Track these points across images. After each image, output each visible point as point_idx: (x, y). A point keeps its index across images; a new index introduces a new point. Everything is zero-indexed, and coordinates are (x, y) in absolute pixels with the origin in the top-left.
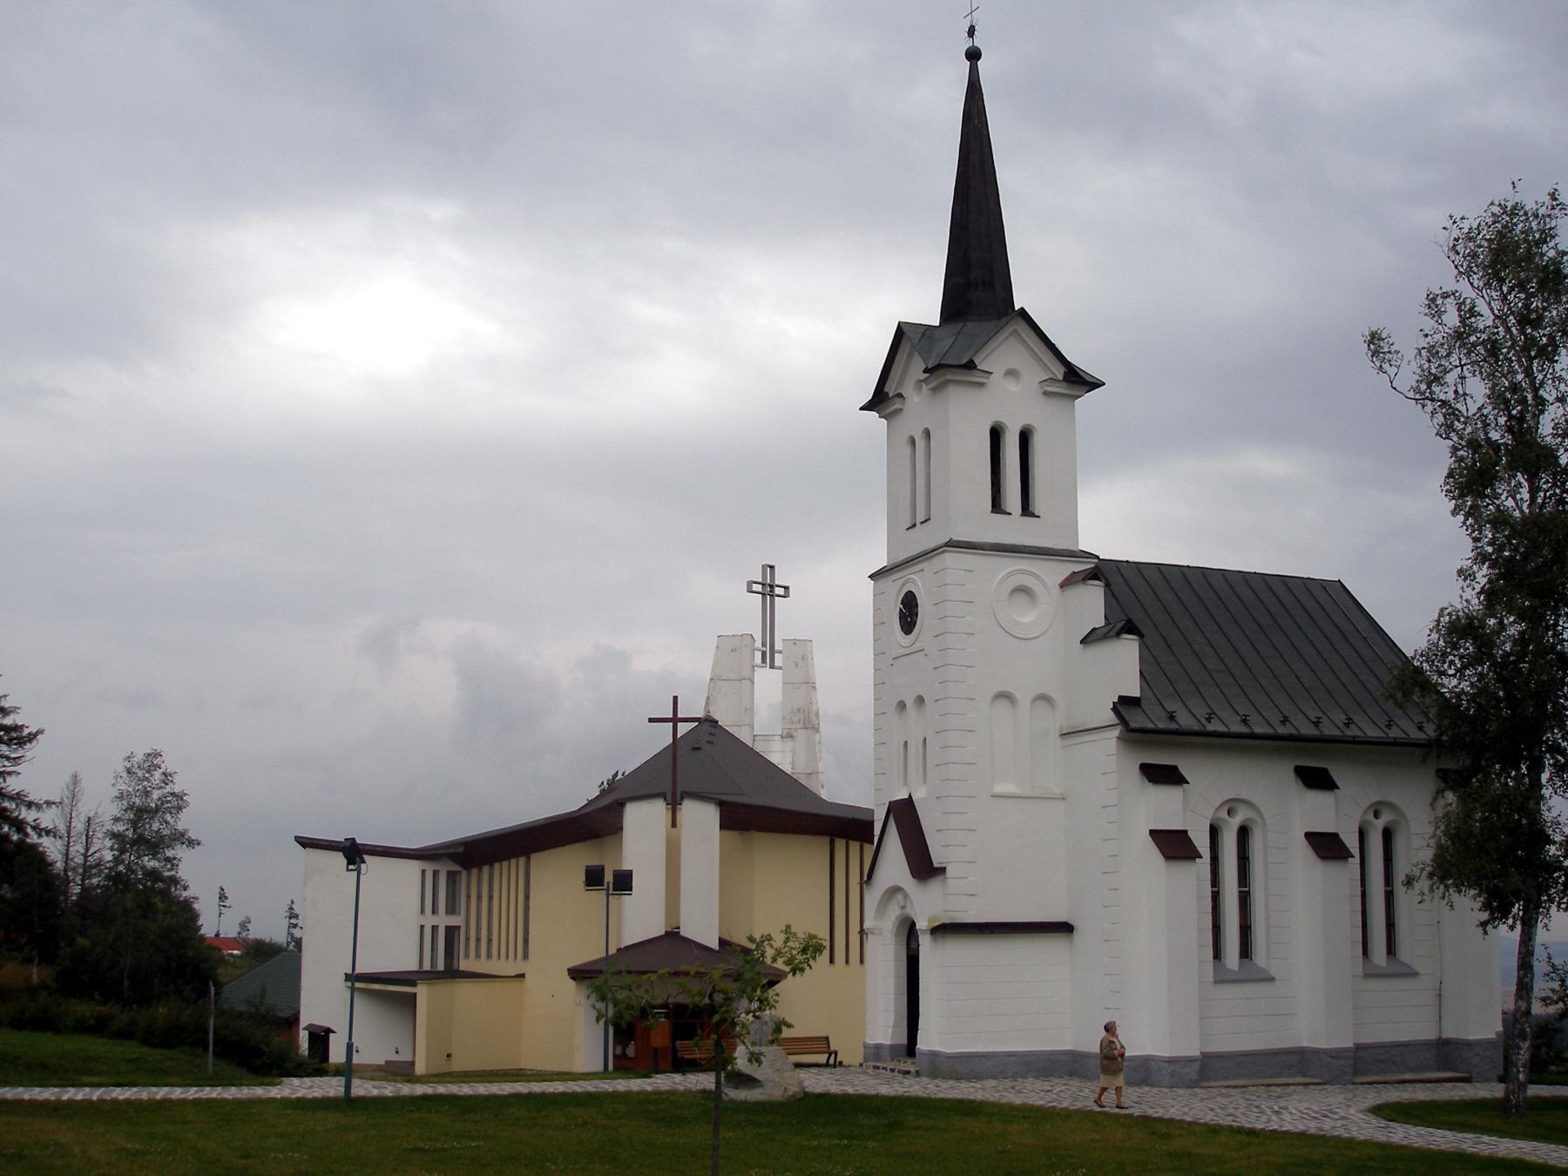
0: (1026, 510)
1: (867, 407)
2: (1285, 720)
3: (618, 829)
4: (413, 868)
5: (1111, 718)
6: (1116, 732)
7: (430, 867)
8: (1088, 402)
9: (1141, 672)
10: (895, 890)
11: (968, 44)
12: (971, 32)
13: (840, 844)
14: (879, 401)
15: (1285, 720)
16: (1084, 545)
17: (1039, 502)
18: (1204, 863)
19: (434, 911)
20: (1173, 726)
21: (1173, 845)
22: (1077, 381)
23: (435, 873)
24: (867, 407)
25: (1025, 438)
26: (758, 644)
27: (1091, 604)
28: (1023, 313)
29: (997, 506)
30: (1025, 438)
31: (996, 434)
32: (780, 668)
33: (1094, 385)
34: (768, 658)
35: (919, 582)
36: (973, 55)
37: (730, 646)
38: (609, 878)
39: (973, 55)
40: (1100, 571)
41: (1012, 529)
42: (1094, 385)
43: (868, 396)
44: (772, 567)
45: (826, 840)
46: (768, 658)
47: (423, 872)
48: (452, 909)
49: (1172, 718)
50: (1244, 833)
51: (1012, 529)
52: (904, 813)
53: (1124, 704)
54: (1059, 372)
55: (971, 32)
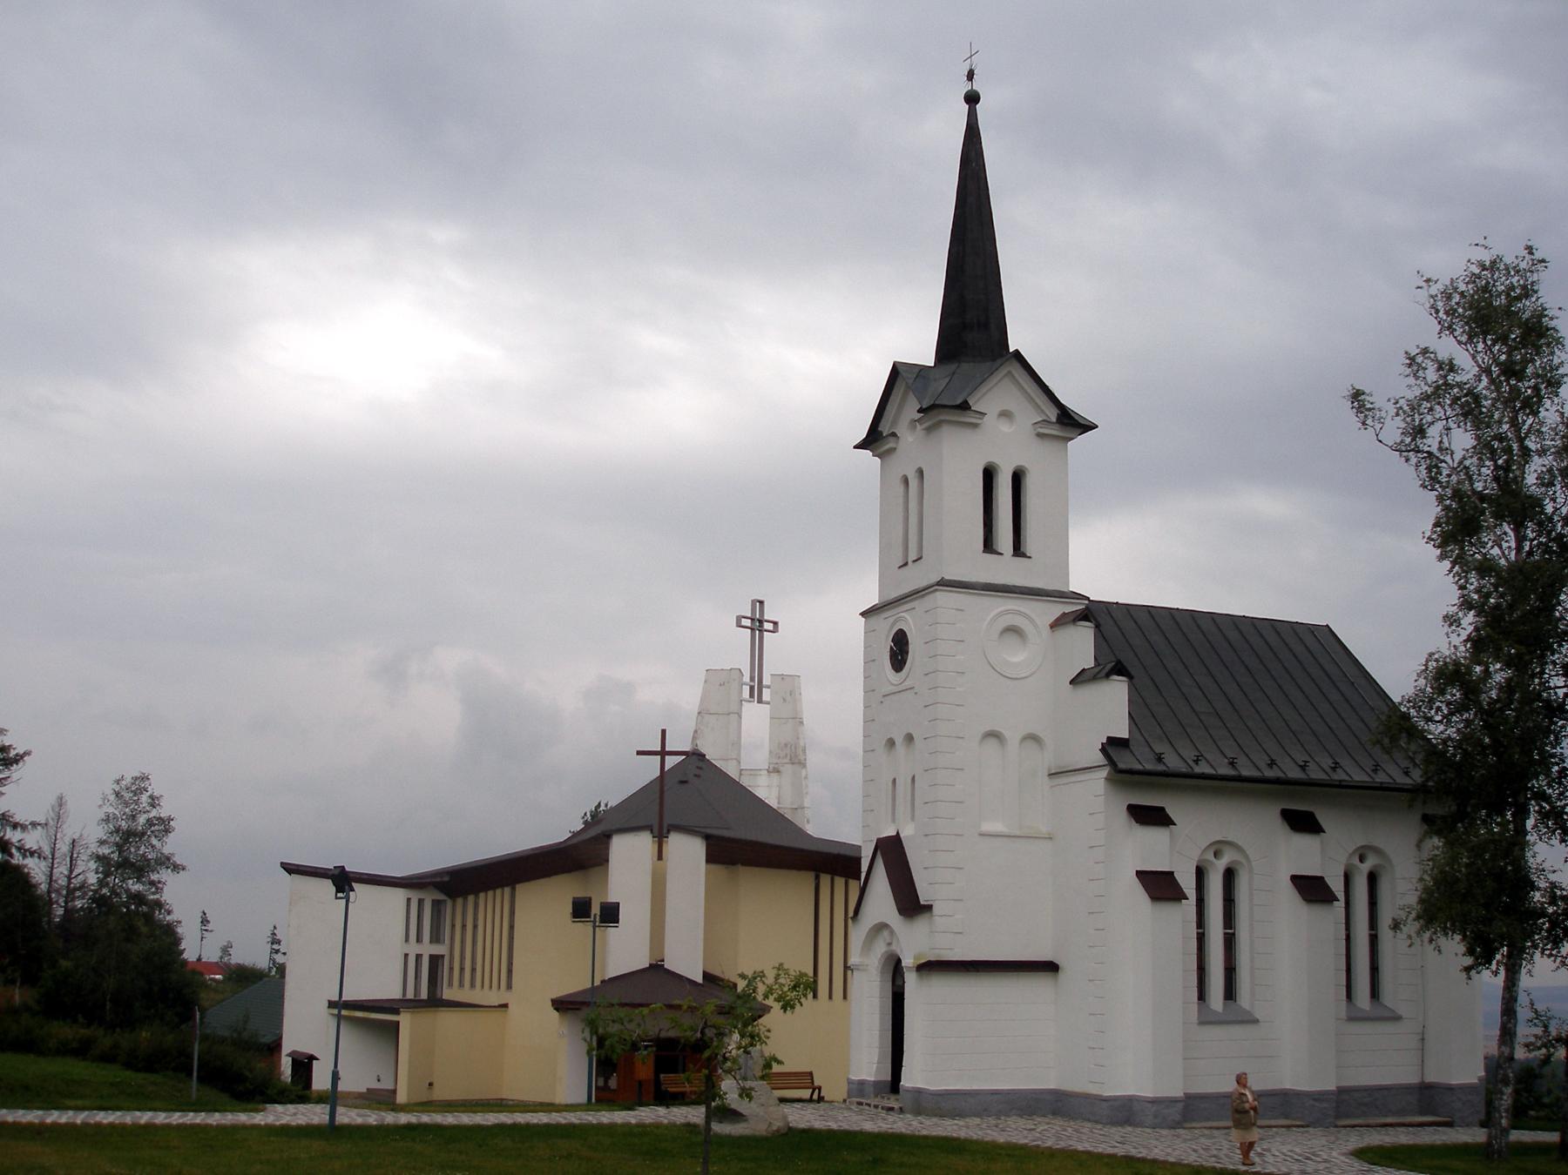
0: (1018, 550)
2: (1272, 764)
3: (604, 860)
4: (398, 896)
5: (1099, 758)
6: (1104, 773)
7: (415, 896)
9: (1129, 713)
11: (966, 87)
12: (971, 76)
13: (825, 880)
14: (874, 439)
15: (1272, 764)
16: (1074, 587)
17: (1031, 542)
19: (419, 940)
20: (1161, 768)
21: (1159, 886)
22: (1070, 423)
23: (421, 902)
25: (1018, 478)
26: (747, 678)
27: (1081, 645)
29: (989, 545)
30: (1018, 478)
31: (989, 475)
32: (768, 703)
33: (1087, 427)
34: (756, 692)
35: (910, 620)
36: (972, 99)
37: (718, 680)
39: (972, 99)
40: (1091, 613)
41: (1004, 569)
42: (1087, 427)
44: (761, 603)
45: (810, 876)
46: (756, 692)
49: (1159, 759)
50: (1230, 875)
51: (1004, 569)
53: (1113, 746)
54: (1053, 414)
55: (971, 76)
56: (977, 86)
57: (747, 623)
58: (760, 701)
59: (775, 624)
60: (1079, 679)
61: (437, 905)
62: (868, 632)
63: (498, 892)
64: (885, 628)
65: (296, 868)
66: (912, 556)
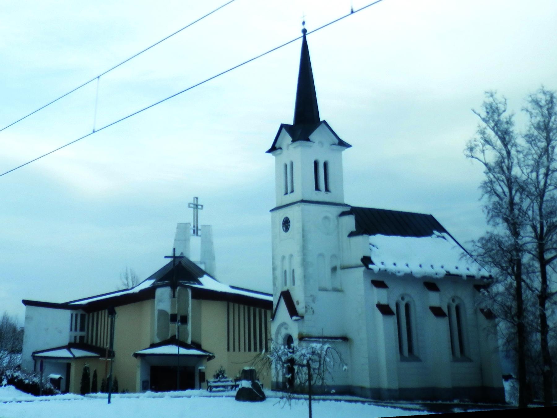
0: (327, 190)
1: (270, 151)
3: (154, 297)
4: (67, 314)
5: (360, 263)
7: (74, 312)
8: (346, 152)
10: (283, 324)
11: (302, 27)
12: (304, 23)
13: (231, 304)
14: (273, 149)
16: (346, 202)
17: (331, 186)
18: (395, 317)
19: (76, 330)
21: (385, 309)
22: (342, 144)
23: (76, 315)
24: (270, 151)
25: (326, 165)
26: (192, 226)
27: (350, 222)
28: (325, 122)
29: (317, 188)
31: (316, 164)
32: (200, 236)
33: (348, 146)
37: (182, 228)
38: (179, 318)
40: (355, 211)
41: (322, 196)
42: (348, 146)
43: (270, 147)
44: (197, 198)
45: (225, 304)
46: (196, 231)
47: (72, 315)
48: (82, 329)
51: (322, 196)
52: (286, 296)
54: (337, 141)
55: (304, 23)
56: (306, 27)
57: (192, 206)
58: (197, 235)
59: (202, 206)
60: (351, 234)
61: (83, 317)
62: (273, 218)
63: (103, 311)
64: (282, 215)
65: (378, 404)
66: (289, 190)
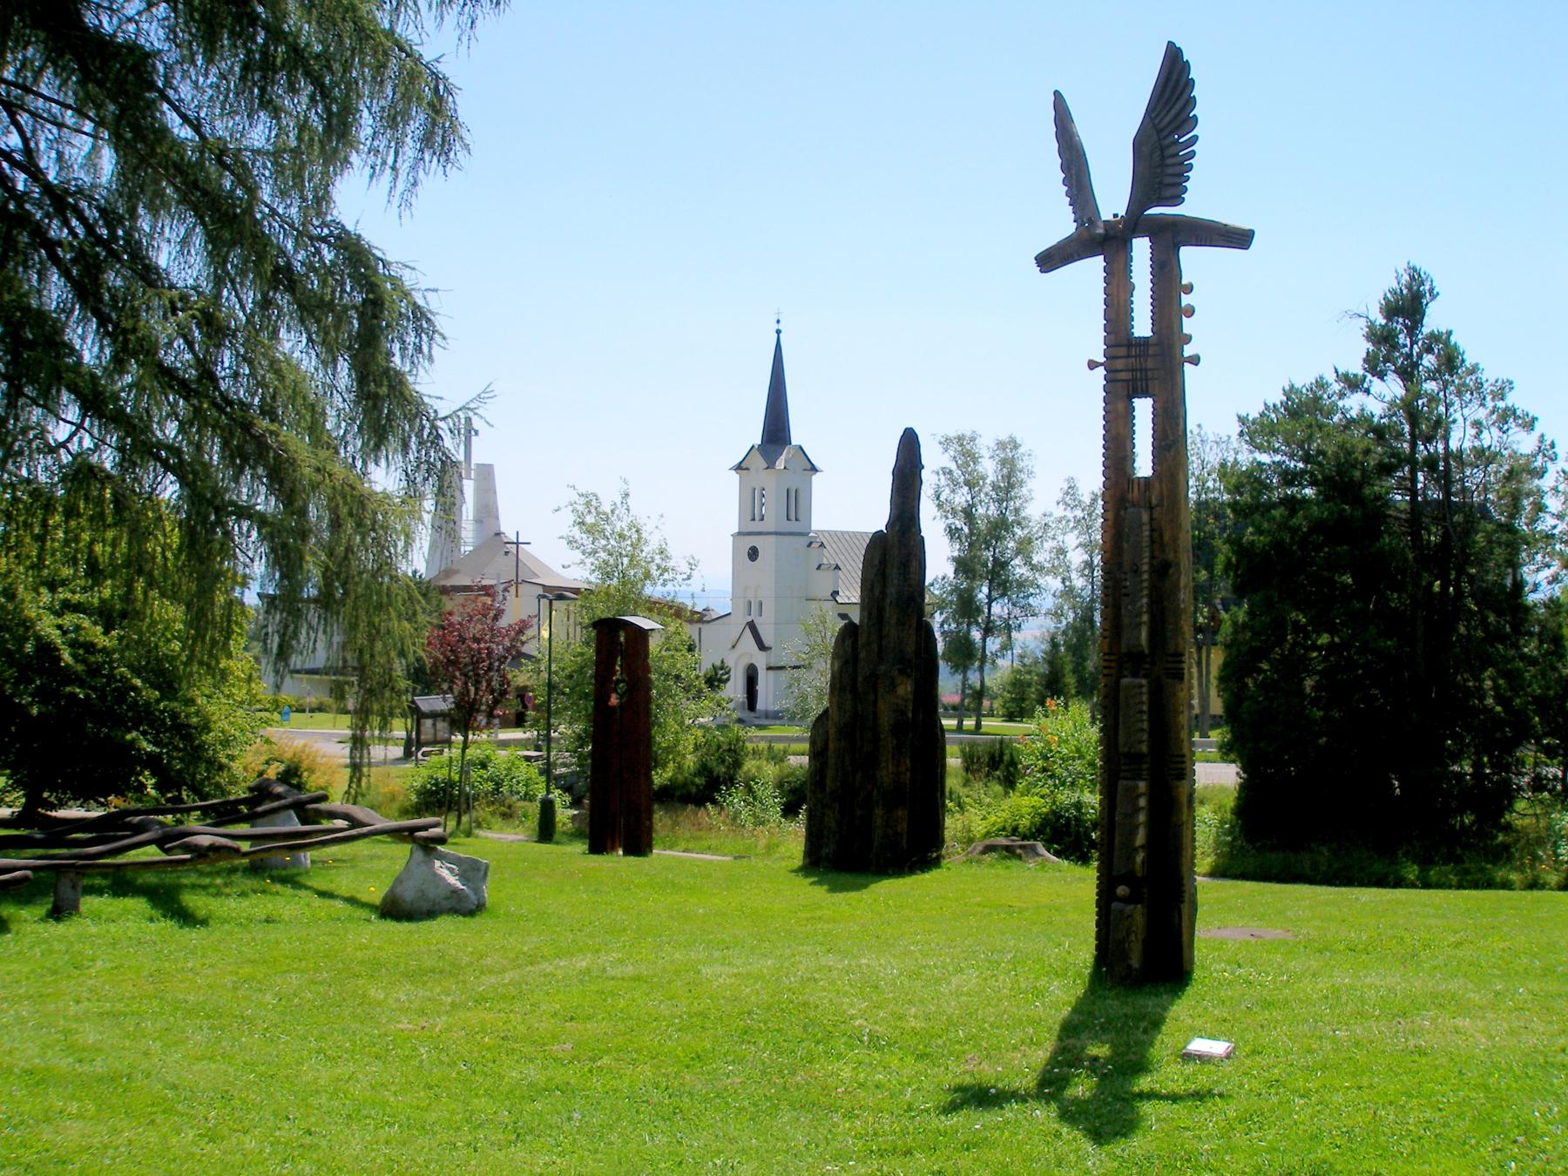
12: (778, 322)
14: (739, 468)
22: (814, 469)
36: (778, 332)
39: (778, 332)
54: (809, 466)
55: (778, 322)
